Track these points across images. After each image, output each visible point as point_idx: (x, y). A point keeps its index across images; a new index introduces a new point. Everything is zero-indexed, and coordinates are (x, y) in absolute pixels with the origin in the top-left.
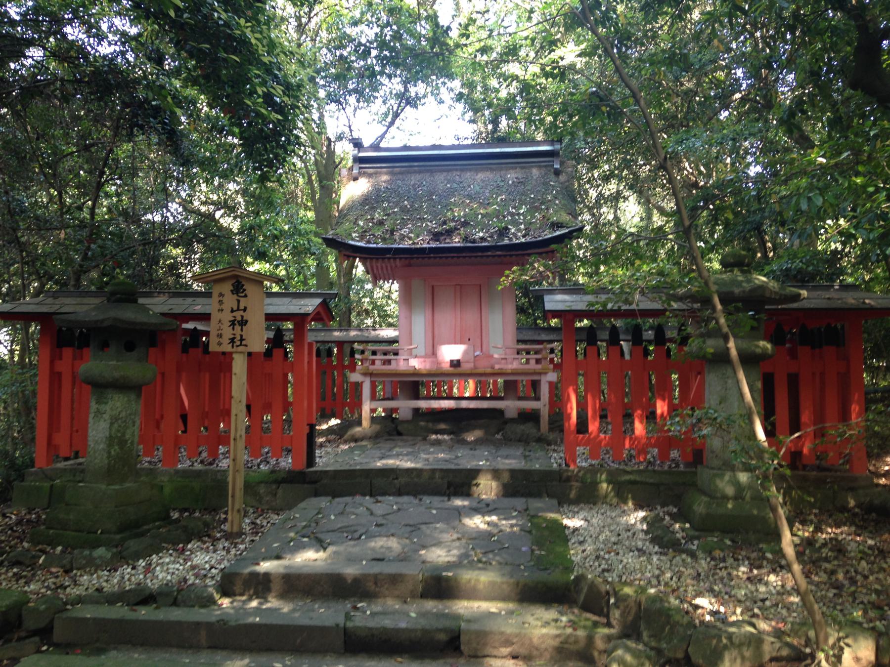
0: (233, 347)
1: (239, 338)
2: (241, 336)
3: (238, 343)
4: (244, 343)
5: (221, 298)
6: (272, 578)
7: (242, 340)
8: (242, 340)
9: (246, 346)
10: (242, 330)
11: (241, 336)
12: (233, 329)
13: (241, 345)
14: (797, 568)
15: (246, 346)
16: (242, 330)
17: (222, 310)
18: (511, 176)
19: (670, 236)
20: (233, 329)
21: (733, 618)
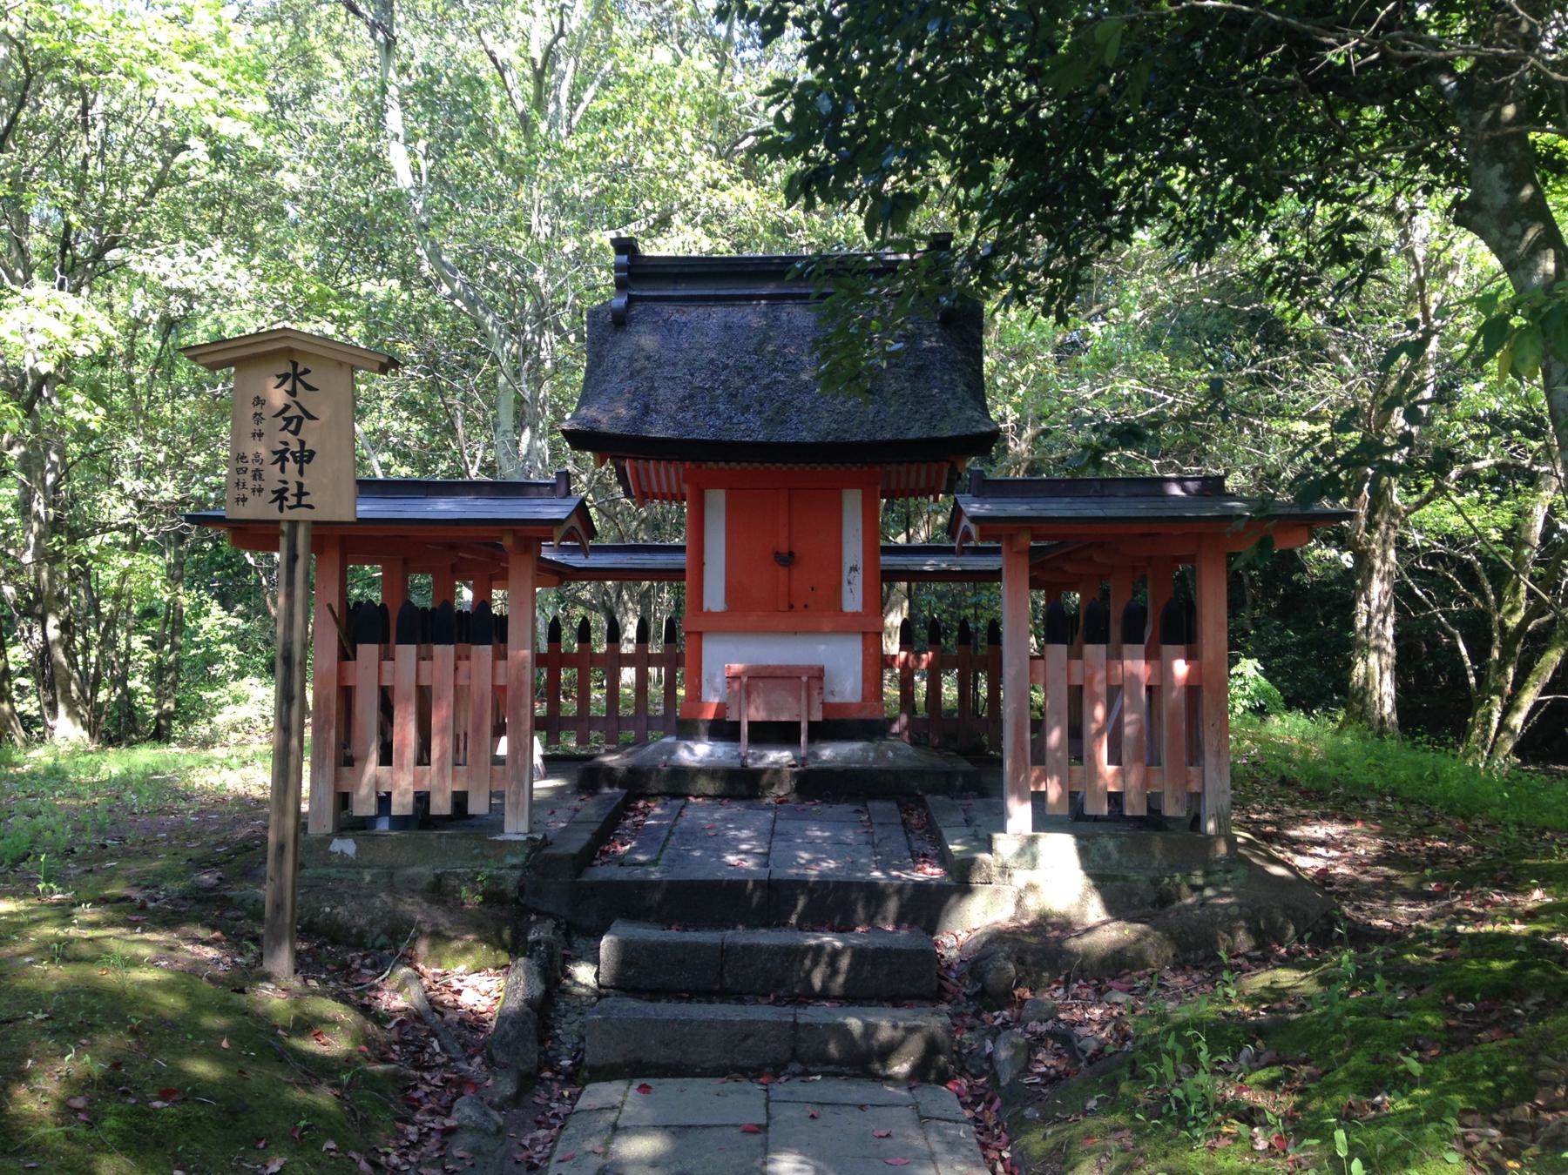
0: (281, 509)
1: (293, 489)
2: (300, 485)
3: (293, 501)
4: (305, 500)
5: (258, 409)
6: (995, 800)
7: (301, 493)
8: (301, 493)
9: (311, 507)
10: (301, 472)
11: (300, 485)
12: (282, 470)
13: (299, 505)
14: (893, 258)
15: (311, 507)
16: (301, 472)
17: (261, 435)
18: (752, 316)
19: (950, 691)
20: (282, 470)
21: (444, 258)
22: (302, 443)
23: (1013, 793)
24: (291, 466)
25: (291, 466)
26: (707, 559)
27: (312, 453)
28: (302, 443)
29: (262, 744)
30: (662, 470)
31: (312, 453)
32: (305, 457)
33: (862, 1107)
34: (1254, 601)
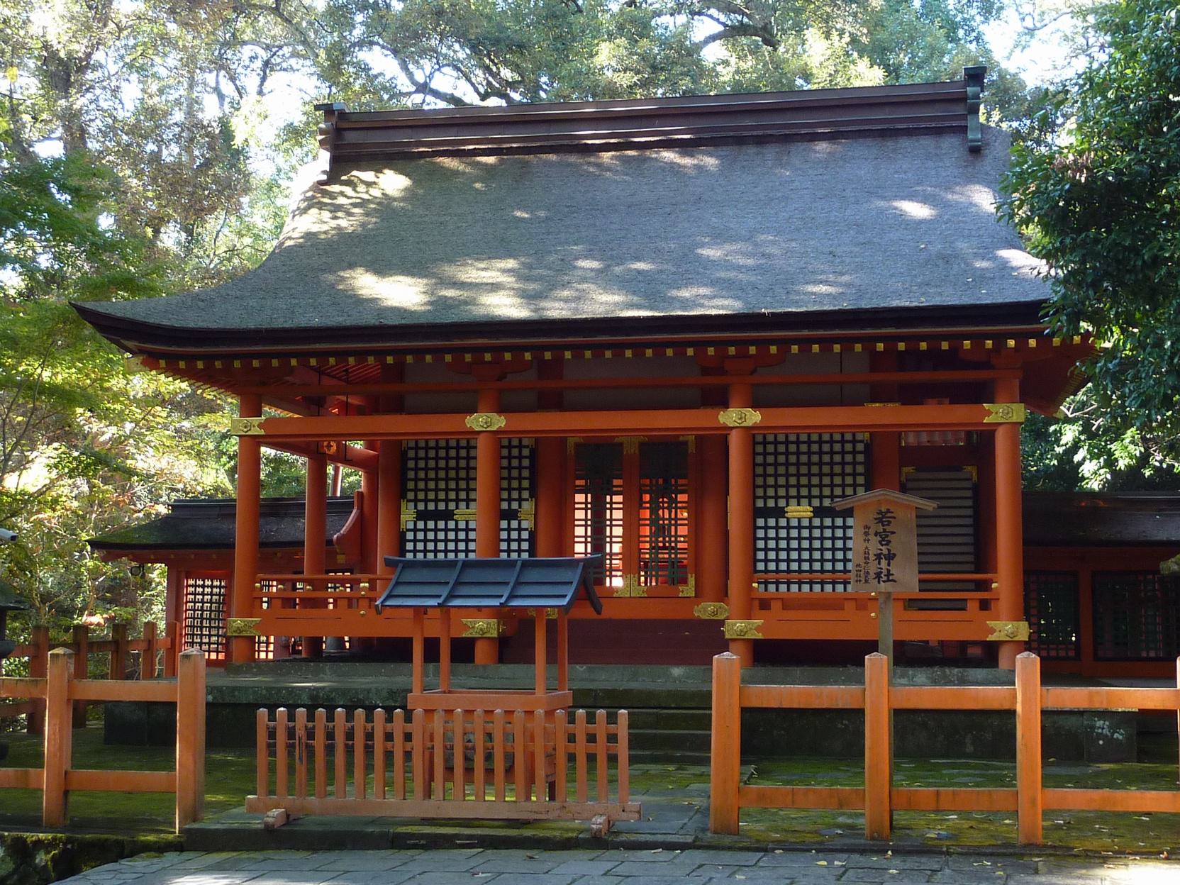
1: (885, 572)
3: (885, 578)
13: (888, 580)
25: (884, 563)
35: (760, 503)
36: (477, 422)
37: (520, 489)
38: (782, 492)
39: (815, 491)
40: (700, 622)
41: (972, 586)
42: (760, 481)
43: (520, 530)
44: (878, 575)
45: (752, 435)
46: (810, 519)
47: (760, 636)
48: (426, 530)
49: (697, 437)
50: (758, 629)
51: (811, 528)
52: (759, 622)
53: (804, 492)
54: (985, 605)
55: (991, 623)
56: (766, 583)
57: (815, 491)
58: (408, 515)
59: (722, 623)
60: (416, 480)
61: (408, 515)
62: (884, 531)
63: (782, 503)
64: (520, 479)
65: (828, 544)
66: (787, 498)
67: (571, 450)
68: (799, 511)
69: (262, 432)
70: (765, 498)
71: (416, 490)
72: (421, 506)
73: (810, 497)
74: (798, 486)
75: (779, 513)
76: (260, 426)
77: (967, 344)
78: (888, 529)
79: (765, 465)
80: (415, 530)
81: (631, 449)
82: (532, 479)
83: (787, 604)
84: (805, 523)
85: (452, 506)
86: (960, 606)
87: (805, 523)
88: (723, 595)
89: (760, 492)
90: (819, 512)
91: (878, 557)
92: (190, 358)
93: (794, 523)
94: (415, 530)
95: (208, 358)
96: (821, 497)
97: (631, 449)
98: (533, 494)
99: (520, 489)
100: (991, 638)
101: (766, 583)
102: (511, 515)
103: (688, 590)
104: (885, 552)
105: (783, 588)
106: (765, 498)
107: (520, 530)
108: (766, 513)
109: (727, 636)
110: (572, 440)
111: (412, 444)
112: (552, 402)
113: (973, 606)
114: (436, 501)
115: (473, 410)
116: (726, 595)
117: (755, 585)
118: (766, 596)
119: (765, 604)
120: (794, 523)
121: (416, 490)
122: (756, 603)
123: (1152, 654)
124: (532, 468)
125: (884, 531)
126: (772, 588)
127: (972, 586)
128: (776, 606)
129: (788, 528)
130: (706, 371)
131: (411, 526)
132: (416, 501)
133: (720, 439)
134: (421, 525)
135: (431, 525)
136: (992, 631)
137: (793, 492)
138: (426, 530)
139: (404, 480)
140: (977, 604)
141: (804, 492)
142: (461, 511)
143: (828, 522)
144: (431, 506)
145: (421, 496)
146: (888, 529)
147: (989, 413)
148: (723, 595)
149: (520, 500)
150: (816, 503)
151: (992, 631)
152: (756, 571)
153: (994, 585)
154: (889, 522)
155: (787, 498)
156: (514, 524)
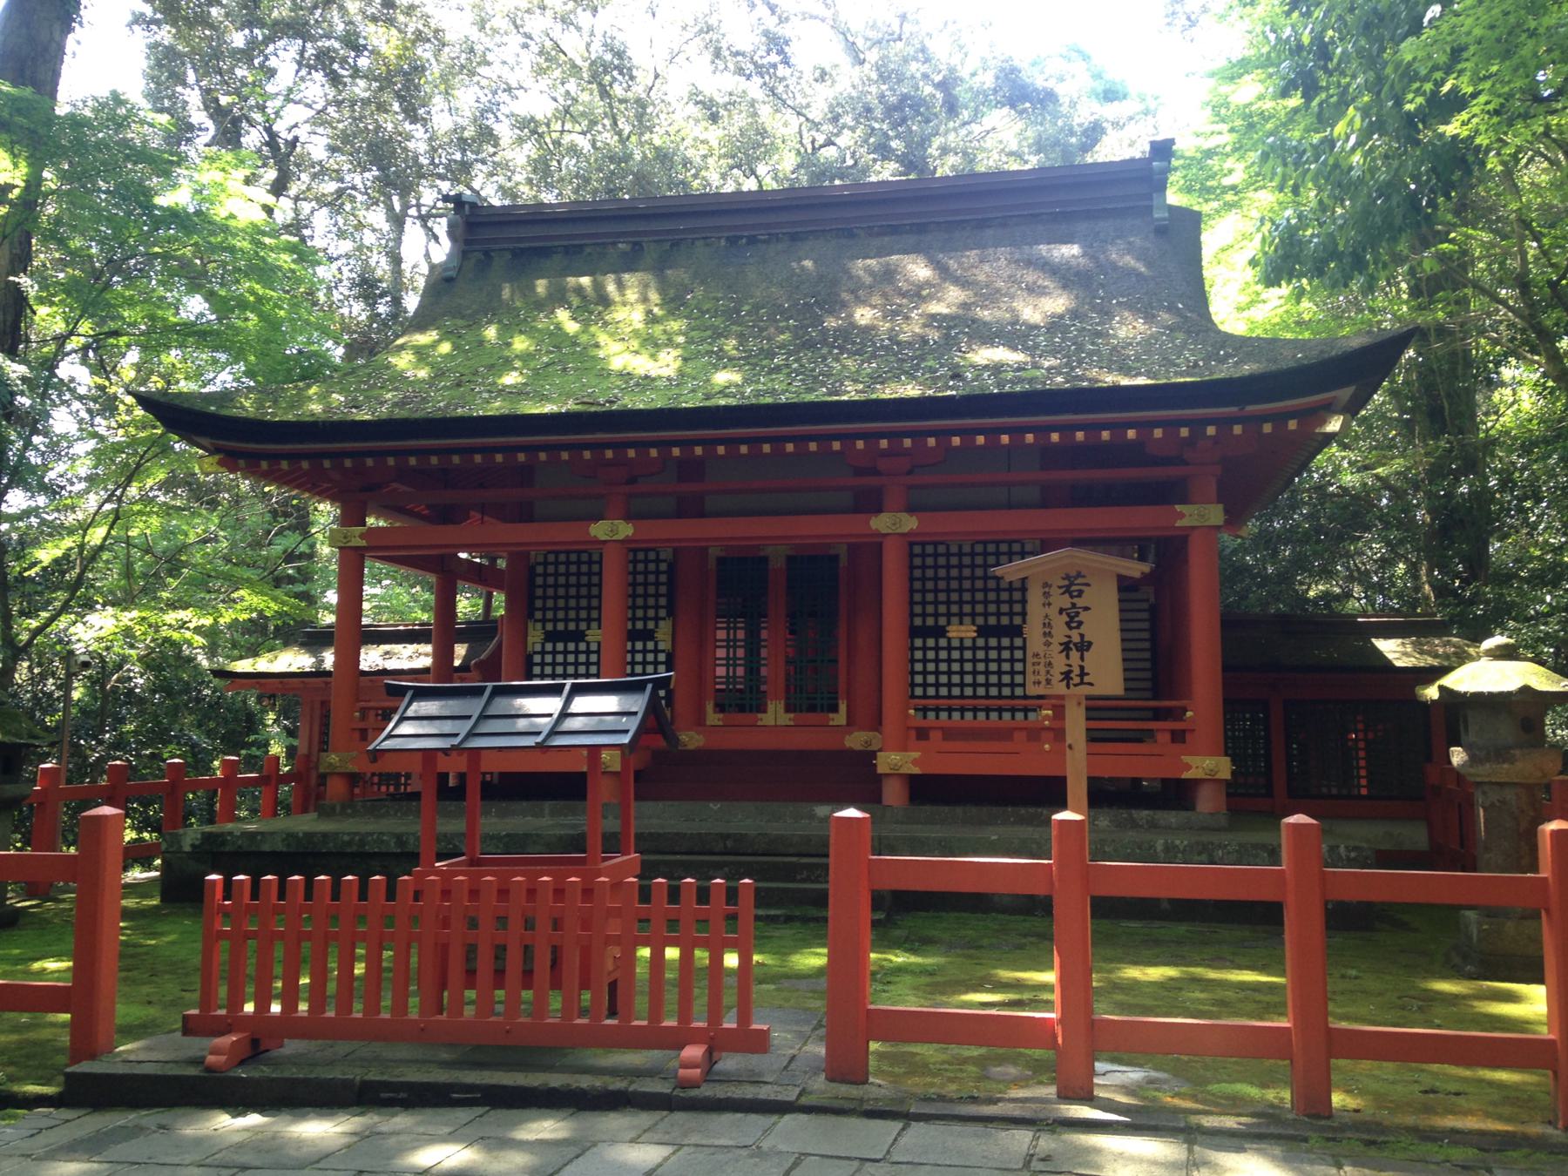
1: (1077, 671)
2: (1082, 668)
3: (1077, 680)
4: (1086, 679)
7: (1083, 674)
8: (1083, 674)
10: (1082, 659)
11: (1082, 668)
12: (1068, 657)
13: (1082, 683)
16: (1082, 659)
20: (1068, 657)
22: (1082, 636)
23: (1338, 1087)
24: (1075, 654)
25: (1075, 654)
26: (885, 670)
27: (1090, 644)
28: (1082, 636)
29: (669, 638)
30: (1145, 606)
31: (1090, 644)
32: (1084, 646)
33: (1464, 1167)
34: (1371, 150)
35: (918, 621)
36: (600, 530)
37: (657, 607)
38: (942, 609)
39: (979, 608)
40: (852, 751)
41: (1150, 714)
42: (918, 597)
43: (656, 651)
44: (1067, 676)
45: (911, 542)
46: (974, 639)
47: (916, 771)
48: (554, 653)
49: (850, 545)
50: (915, 762)
51: (974, 648)
52: (916, 755)
53: (967, 609)
54: (1178, 737)
55: (1186, 759)
56: (925, 710)
57: (979, 608)
58: (535, 637)
59: (873, 755)
60: (545, 598)
61: (535, 637)
62: (1074, 605)
63: (942, 621)
64: (657, 596)
65: (993, 667)
66: (949, 615)
67: (712, 564)
68: (962, 631)
69: (363, 543)
70: (924, 615)
71: (544, 609)
72: (549, 627)
73: (973, 615)
74: (961, 602)
75: (940, 632)
76: (362, 536)
77: (1158, 433)
78: (1080, 602)
79: (924, 567)
80: (543, 653)
81: (778, 563)
82: (671, 596)
83: (949, 734)
84: (968, 643)
85: (583, 626)
86: (1138, 737)
87: (968, 643)
88: (876, 723)
89: (918, 609)
90: (983, 631)
91: (1066, 647)
92: (275, 457)
93: (956, 643)
94: (543, 653)
95: (294, 457)
96: (986, 615)
97: (778, 563)
98: (671, 613)
99: (657, 607)
100: (1186, 775)
101: (925, 710)
102: (648, 635)
103: (840, 718)
104: (1076, 639)
105: (944, 715)
106: (924, 615)
107: (656, 651)
108: (924, 632)
109: (880, 770)
110: (714, 552)
111: (541, 559)
112: (690, 508)
113: (1164, 738)
114: (566, 620)
115: (597, 518)
116: (880, 724)
117: (912, 712)
118: (924, 724)
119: (922, 734)
120: (956, 643)
121: (544, 609)
122: (913, 733)
123: (1334, 791)
124: (671, 583)
125: (1074, 605)
126: (931, 715)
127: (1150, 714)
128: (935, 736)
129: (949, 648)
130: (859, 472)
131: (538, 648)
132: (544, 621)
133: (874, 547)
134: (549, 647)
135: (560, 646)
136: (1188, 767)
137: (955, 609)
138: (554, 653)
139: (531, 598)
140: (1168, 736)
141: (967, 609)
142: (594, 635)
143: (993, 642)
144: (561, 626)
145: (550, 615)
146: (1080, 602)
147: (1182, 516)
148: (876, 723)
149: (657, 619)
150: (980, 621)
151: (1188, 767)
152: (913, 696)
153: (1189, 714)
154: (1080, 593)
155: (949, 615)
156: (650, 645)
